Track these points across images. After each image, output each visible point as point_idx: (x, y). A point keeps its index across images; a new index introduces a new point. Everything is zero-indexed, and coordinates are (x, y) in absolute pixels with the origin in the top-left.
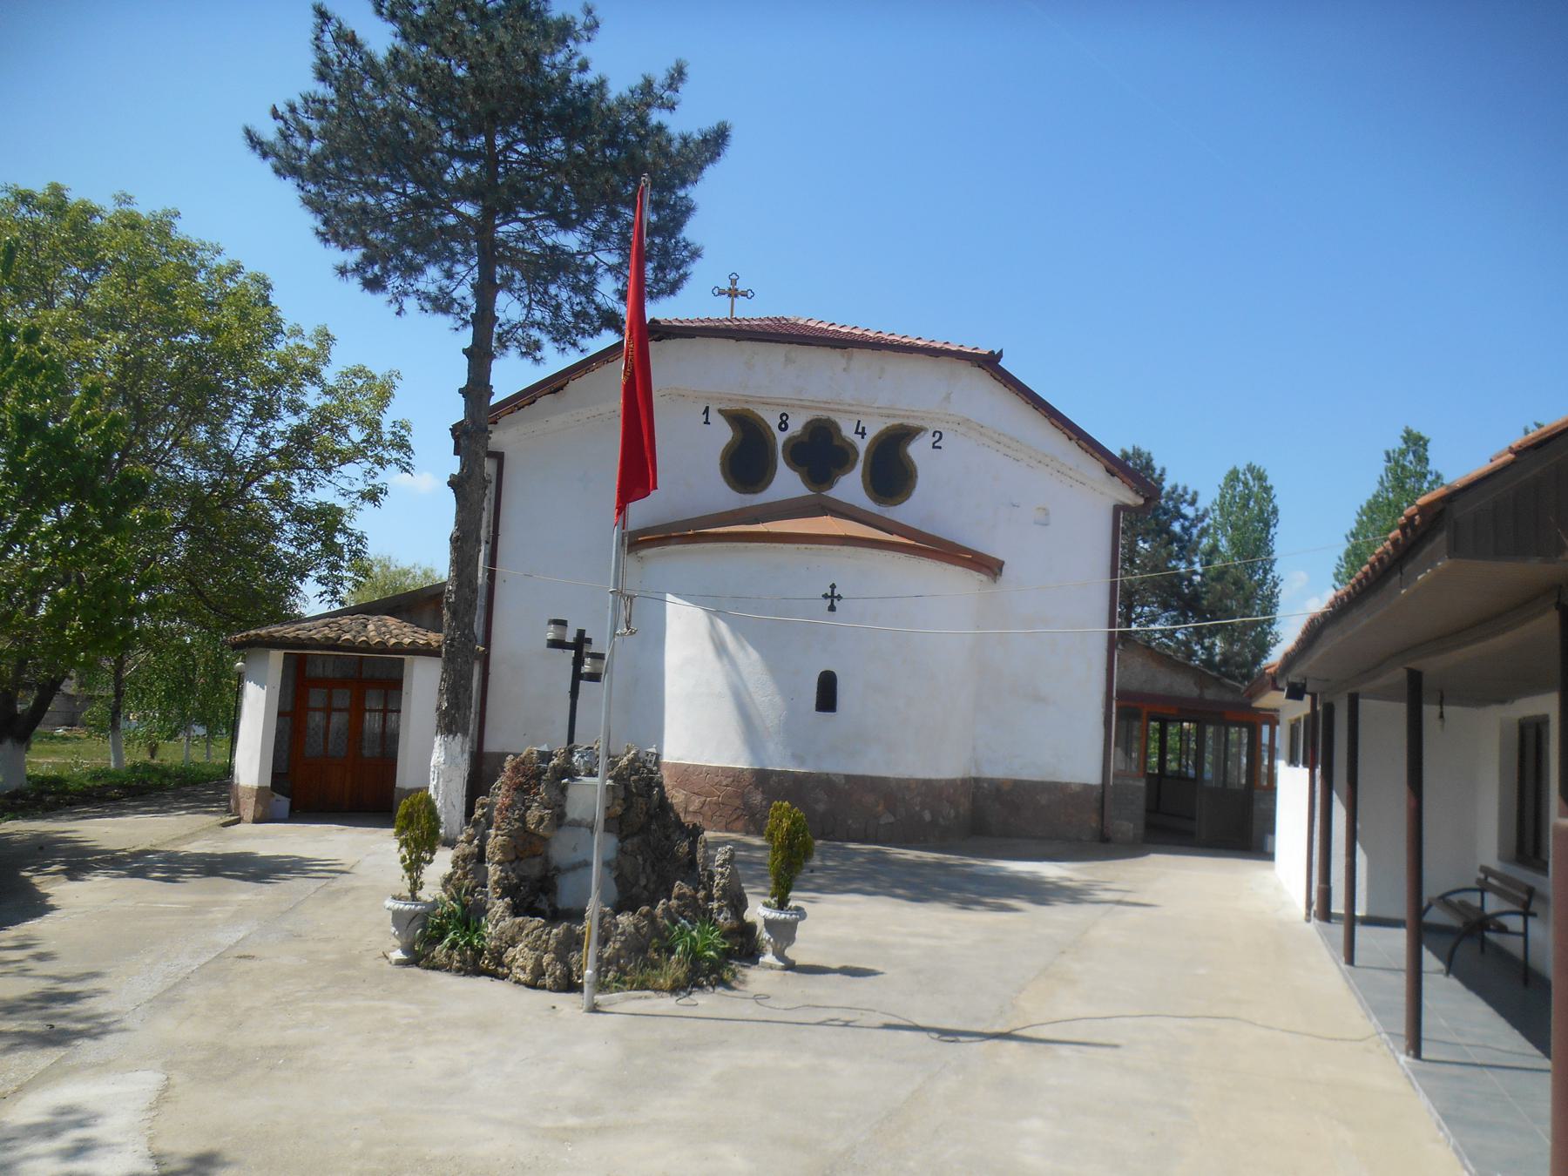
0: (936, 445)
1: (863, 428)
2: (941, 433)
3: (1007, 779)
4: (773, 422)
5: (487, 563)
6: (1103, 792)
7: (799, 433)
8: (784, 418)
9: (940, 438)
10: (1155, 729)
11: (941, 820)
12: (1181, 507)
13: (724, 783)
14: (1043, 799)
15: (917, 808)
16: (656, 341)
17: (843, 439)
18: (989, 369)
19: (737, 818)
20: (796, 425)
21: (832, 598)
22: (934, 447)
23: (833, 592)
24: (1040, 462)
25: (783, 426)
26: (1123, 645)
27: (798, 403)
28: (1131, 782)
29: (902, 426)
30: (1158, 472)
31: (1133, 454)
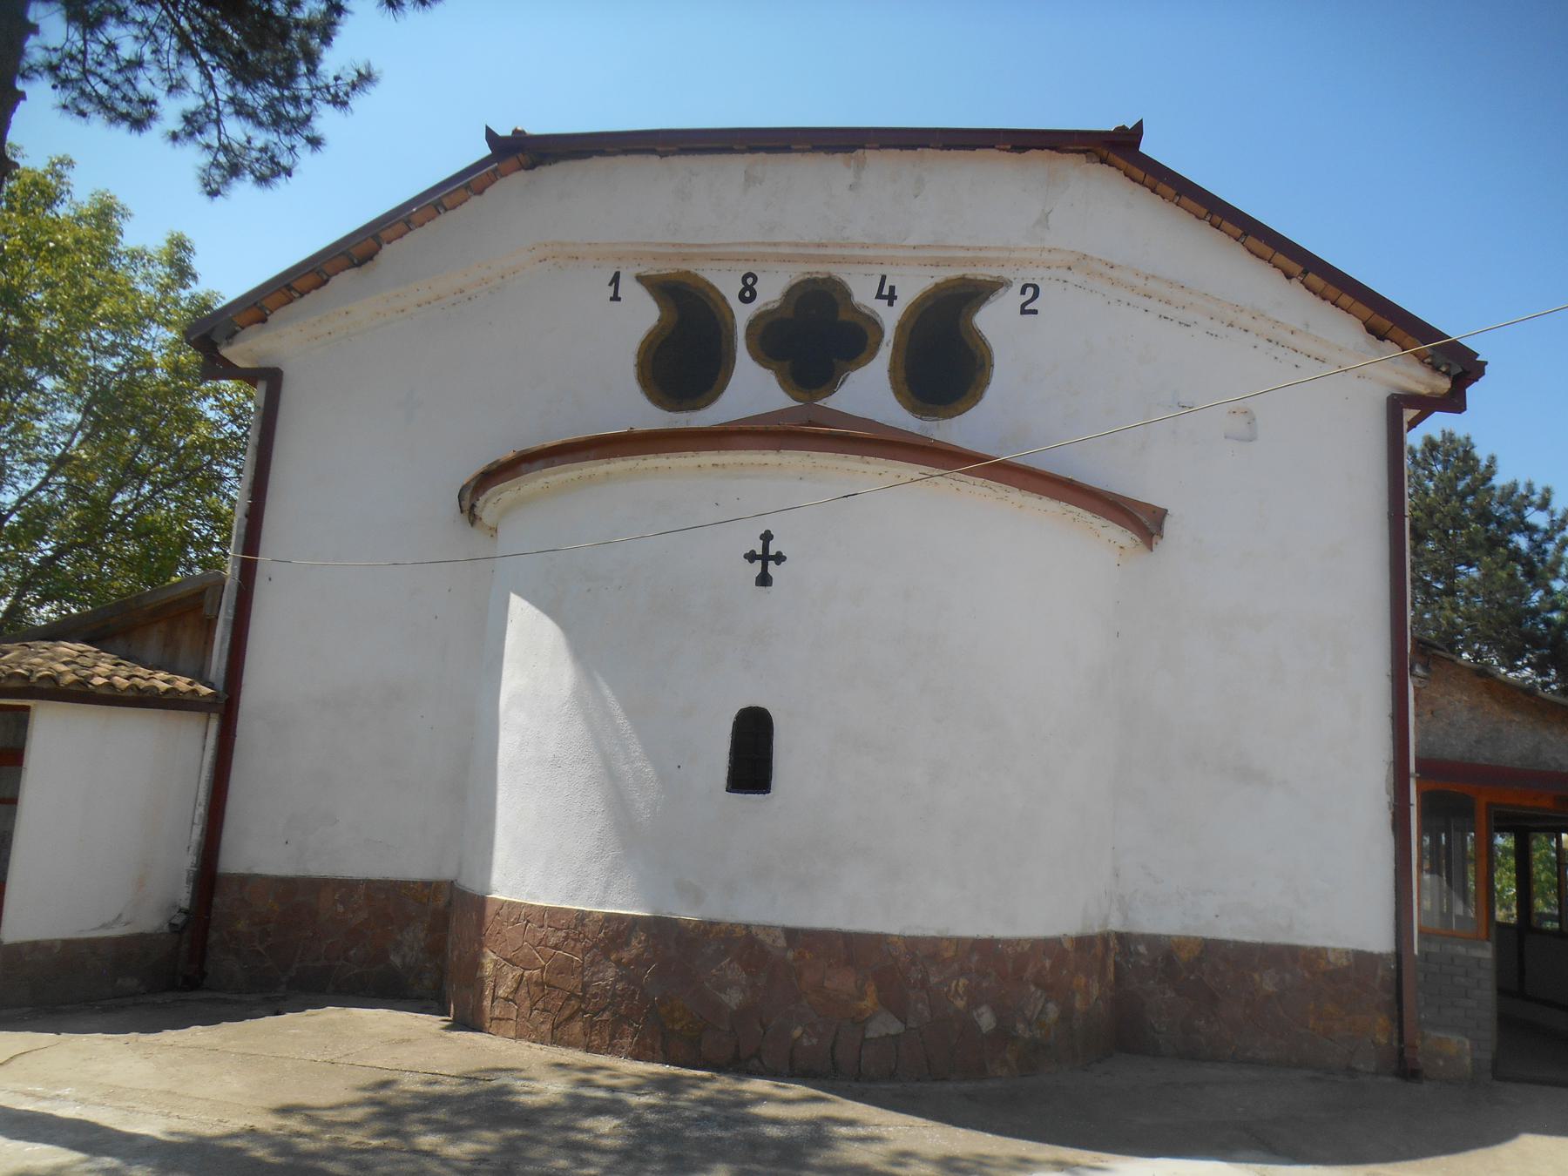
0: (1026, 308)
1: (892, 289)
2: (1036, 288)
3: (1188, 939)
4: (728, 286)
5: (240, 549)
6: (1399, 971)
7: (776, 305)
8: (750, 281)
9: (1036, 295)
10: (1505, 851)
11: (1020, 1027)
12: (1527, 513)
13: (553, 941)
14: (1268, 983)
15: (960, 1003)
16: (527, 169)
17: (855, 310)
18: (1119, 161)
19: (571, 1018)
20: (771, 292)
21: (765, 559)
22: (1023, 312)
23: (766, 548)
24: (1231, 325)
25: (747, 295)
26: (1426, 667)
27: (770, 250)
28: (1461, 950)
29: (964, 281)
30: (1484, 463)
31: (1443, 441)
